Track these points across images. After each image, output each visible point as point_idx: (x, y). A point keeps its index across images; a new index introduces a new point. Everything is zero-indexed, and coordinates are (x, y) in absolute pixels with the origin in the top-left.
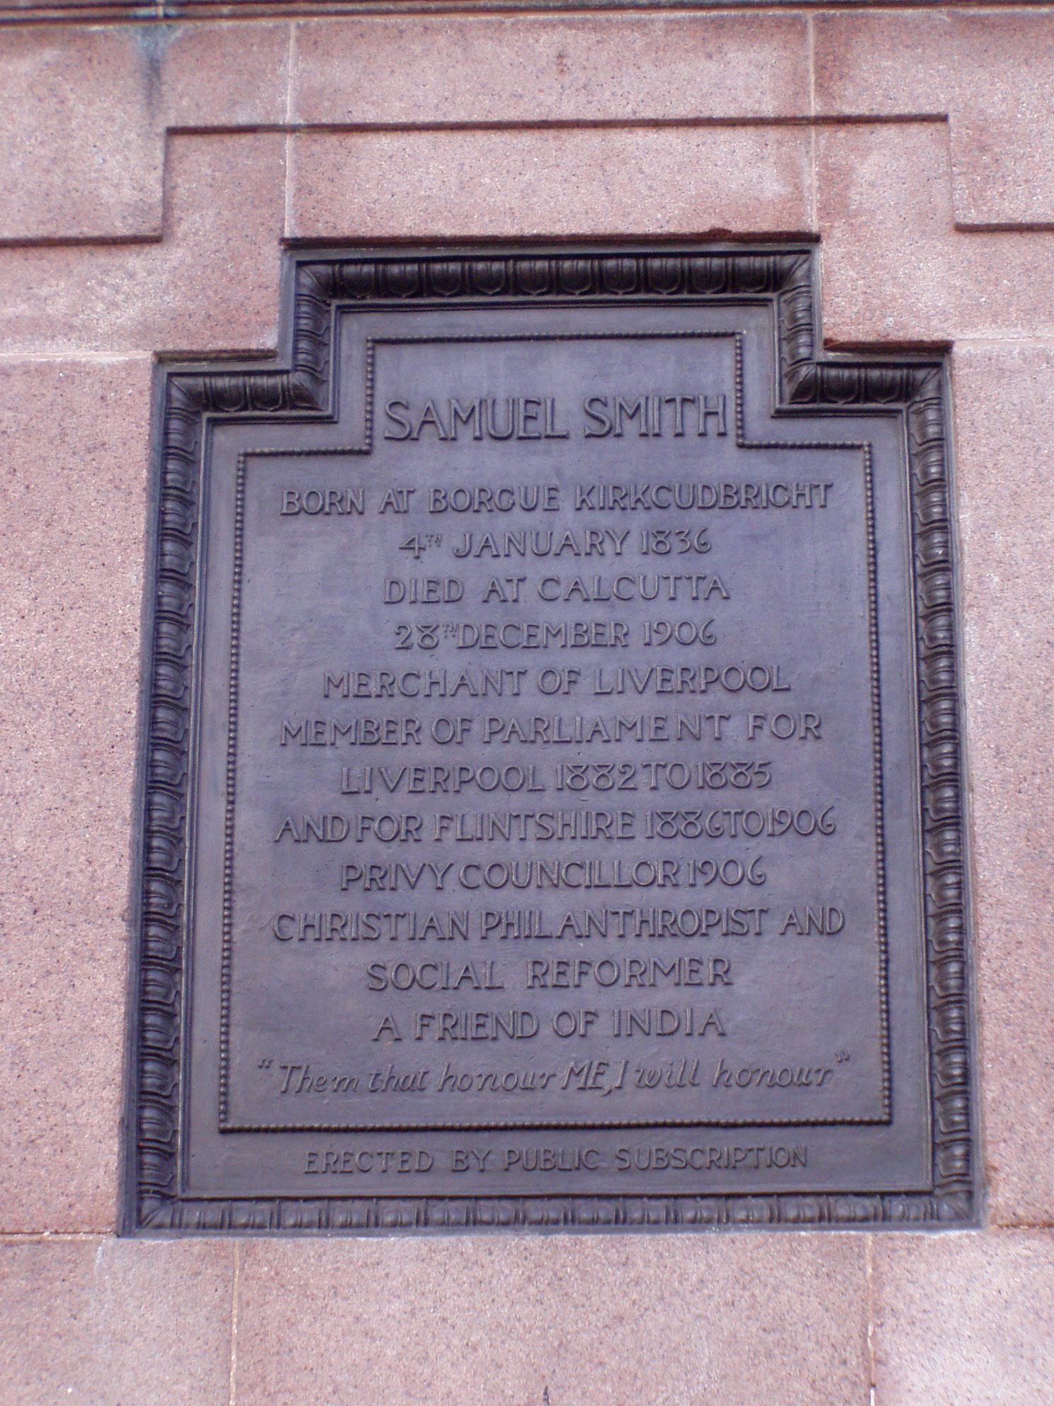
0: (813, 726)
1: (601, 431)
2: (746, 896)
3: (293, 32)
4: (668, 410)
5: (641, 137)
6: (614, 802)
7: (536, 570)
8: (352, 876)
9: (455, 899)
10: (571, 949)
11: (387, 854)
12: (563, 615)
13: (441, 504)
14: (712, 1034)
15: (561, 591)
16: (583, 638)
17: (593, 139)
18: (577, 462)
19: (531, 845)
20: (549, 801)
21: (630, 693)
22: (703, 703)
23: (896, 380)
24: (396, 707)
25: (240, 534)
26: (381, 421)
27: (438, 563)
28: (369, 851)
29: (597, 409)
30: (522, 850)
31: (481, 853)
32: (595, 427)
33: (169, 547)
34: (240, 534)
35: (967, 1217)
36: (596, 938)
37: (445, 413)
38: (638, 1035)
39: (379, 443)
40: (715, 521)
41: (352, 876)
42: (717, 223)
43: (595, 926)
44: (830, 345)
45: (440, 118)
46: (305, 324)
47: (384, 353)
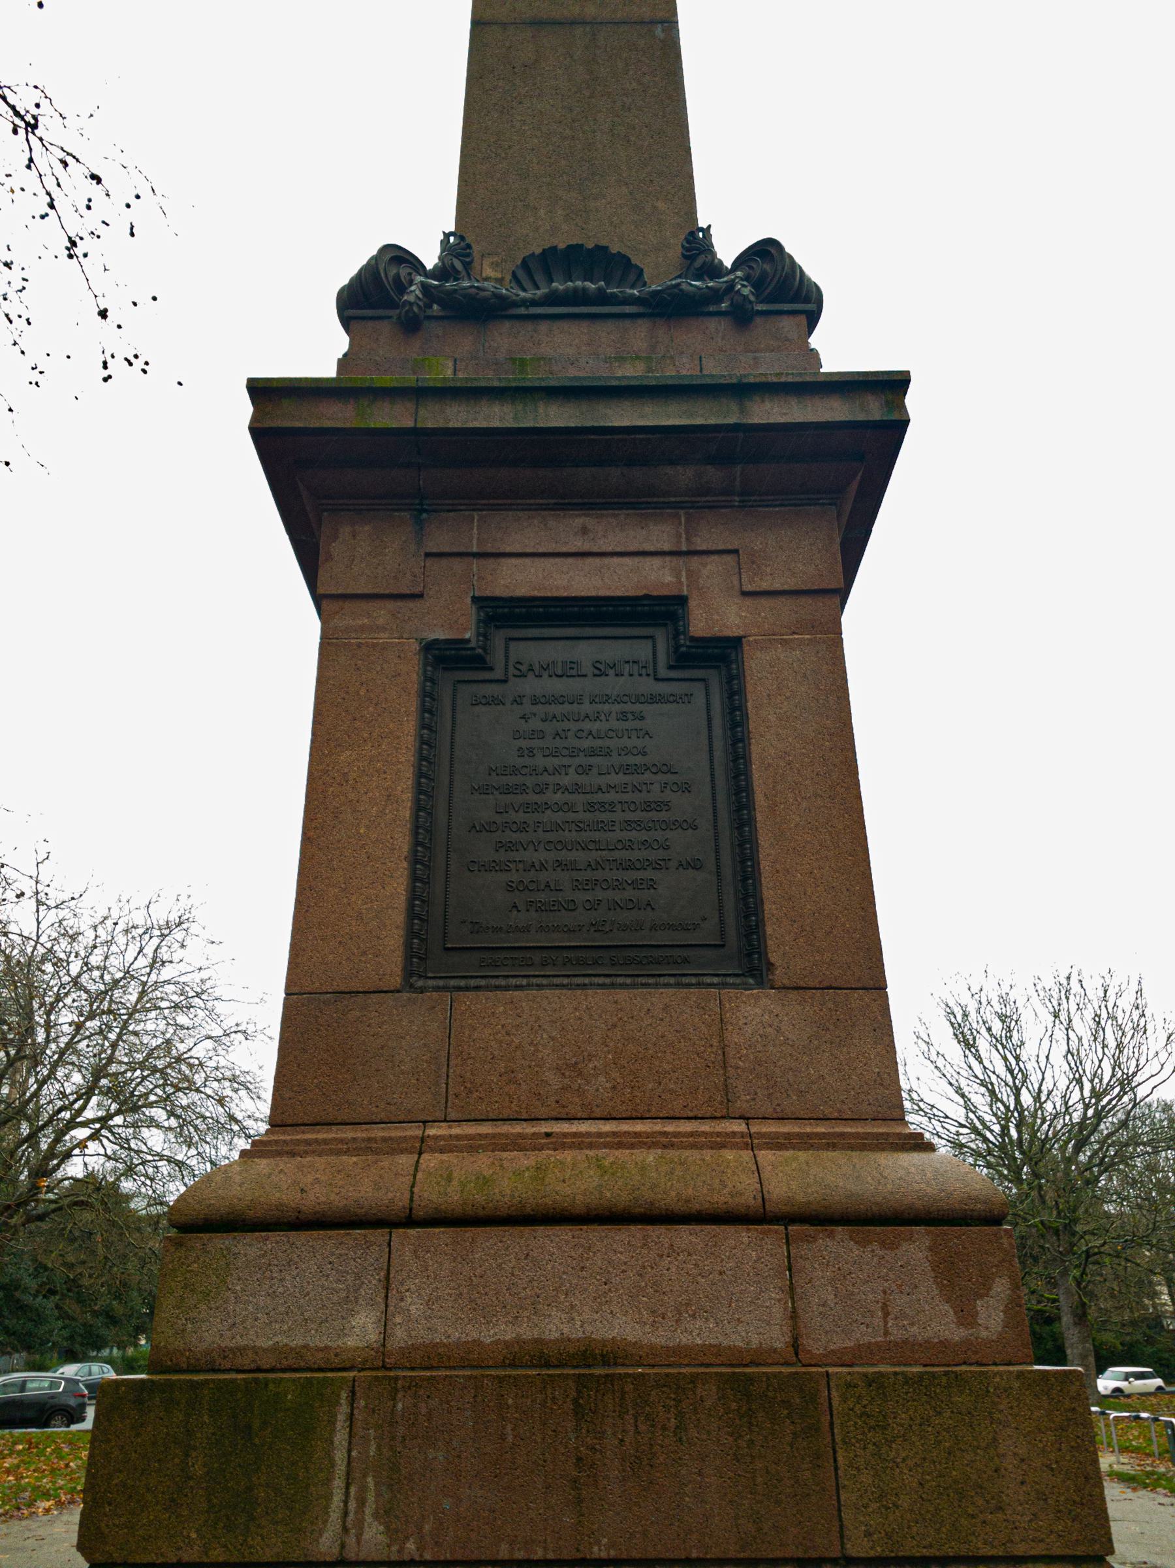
0: (686, 788)
1: (600, 673)
2: (661, 854)
3: (476, 517)
4: (627, 666)
5: (616, 560)
6: (606, 816)
7: (573, 726)
8: (500, 846)
9: (542, 855)
10: (589, 874)
11: (515, 837)
12: (587, 743)
13: (535, 701)
14: (649, 909)
15: (584, 734)
16: (593, 752)
17: (597, 561)
18: (590, 685)
19: (574, 833)
20: (581, 816)
21: (613, 774)
22: (642, 778)
23: (721, 655)
24: (518, 779)
25: (454, 710)
26: (512, 670)
27: (535, 724)
28: (510, 836)
29: (598, 665)
30: (570, 836)
31: (550, 836)
32: (597, 672)
33: (427, 715)
34: (454, 710)
35: (761, 984)
36: (600, 870)
37: (536, 667)
38: (619, 909)
39: (511, 678)
40: (647, 709)
41: (500, 846)
42: (645, 592)
43: (598, 865)
44: (693, 639)
45: (535, 551)
46: (481, 630)
47: (512, 645)
